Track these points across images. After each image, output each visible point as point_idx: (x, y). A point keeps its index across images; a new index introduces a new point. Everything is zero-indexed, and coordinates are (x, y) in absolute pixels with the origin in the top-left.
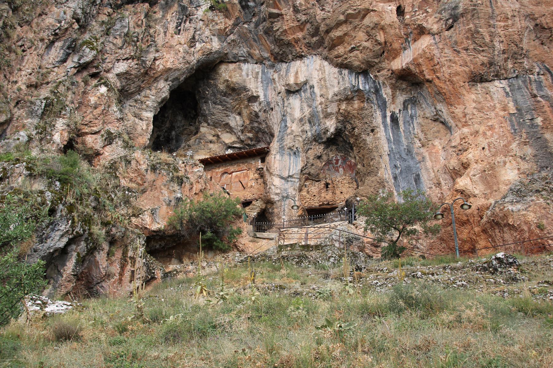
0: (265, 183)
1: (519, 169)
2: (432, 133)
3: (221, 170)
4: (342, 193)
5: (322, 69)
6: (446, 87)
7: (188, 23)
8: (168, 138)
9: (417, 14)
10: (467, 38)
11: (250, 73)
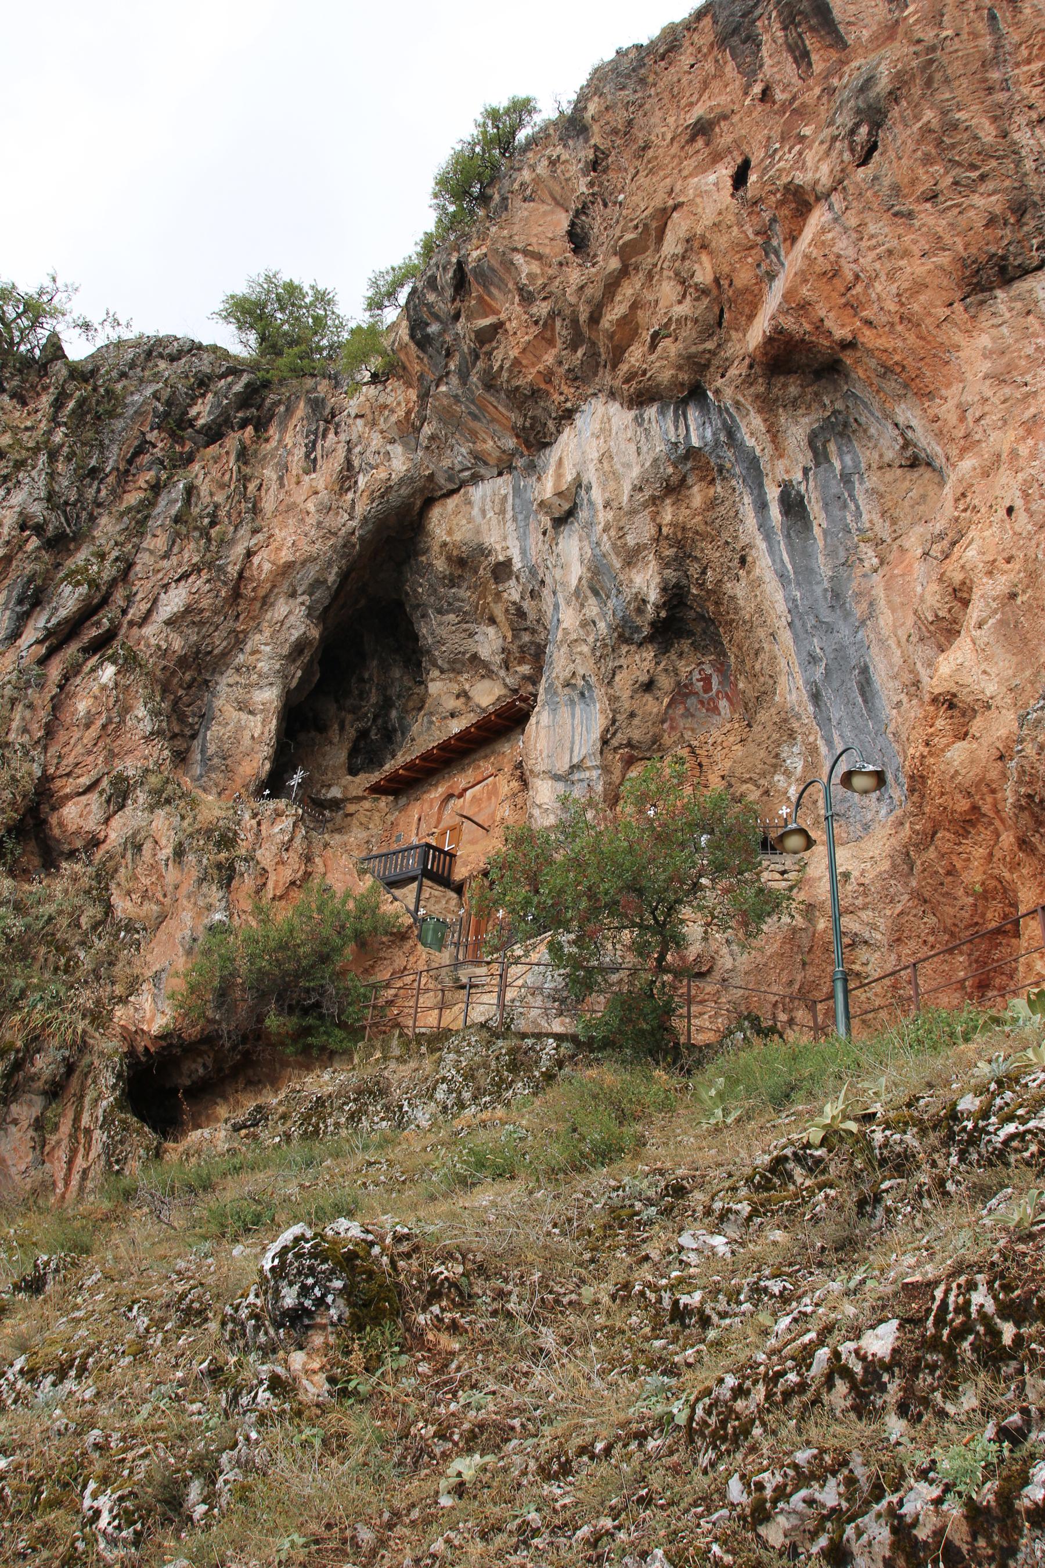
2: (907, 509)
3: (438, 792)
6: (900, 344)
7: (331, 435)
8: (386, 729)
9: (777, 158)
10: (927, 160)
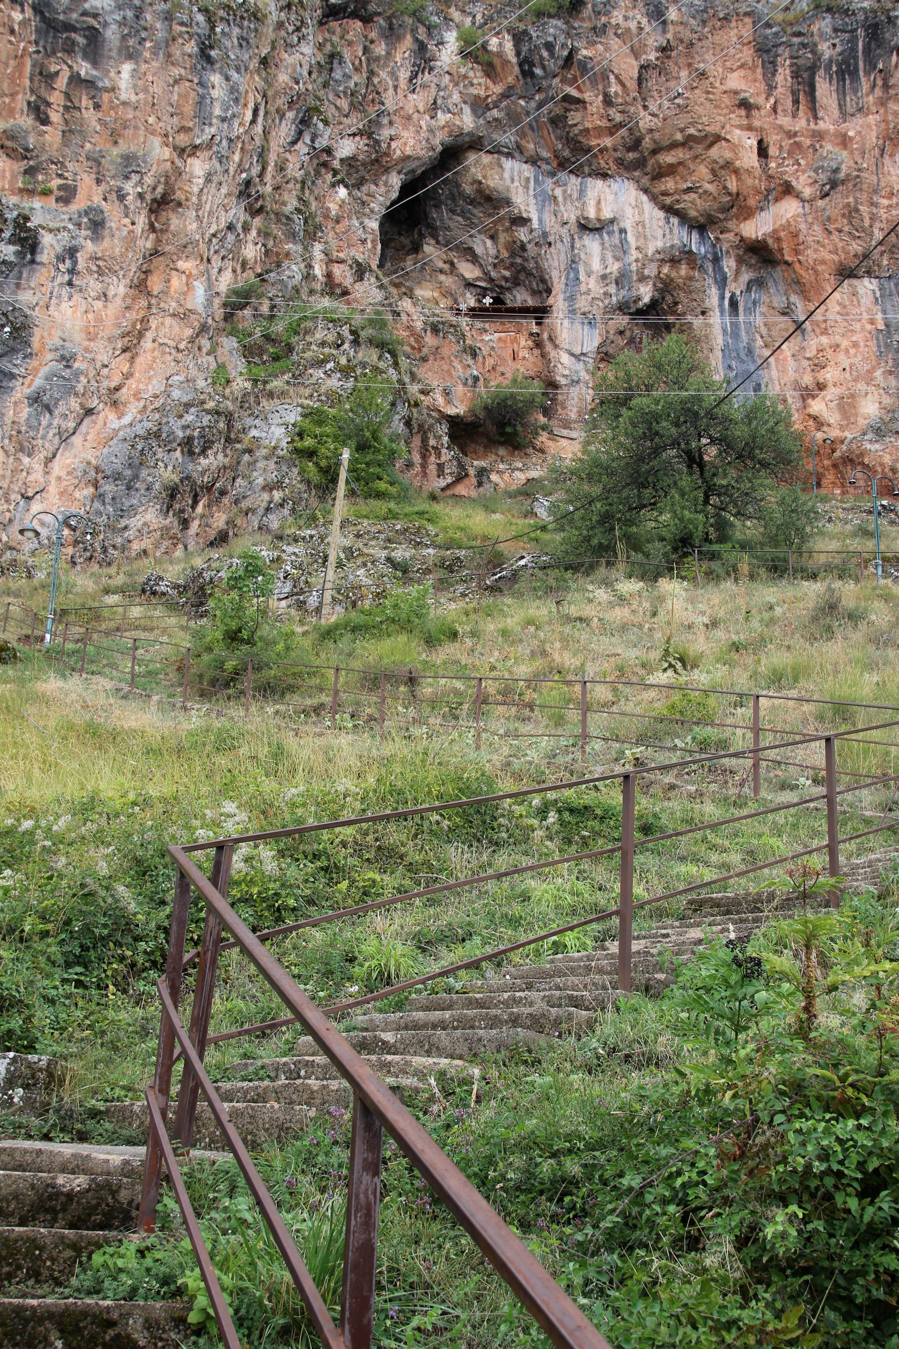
0: (543, 355)
1: (880, 403)
5: (638, 206)
10: (843, 216)
11: (516, 178)
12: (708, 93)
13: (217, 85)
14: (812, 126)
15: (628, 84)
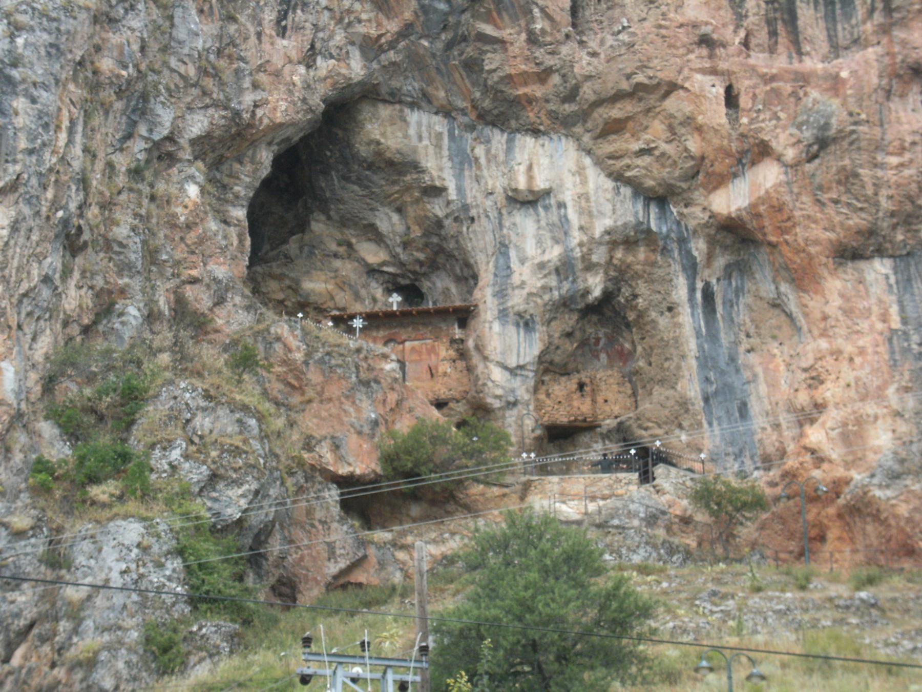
0: (470, 369)
1: (894, 431)
4: (606, 401)
5: (580, 171)
10: (839, 182)
11: (425, 134)
12: (660, 27)
13: (21, 112)
14: (796, 65)
15: (558, 18)
